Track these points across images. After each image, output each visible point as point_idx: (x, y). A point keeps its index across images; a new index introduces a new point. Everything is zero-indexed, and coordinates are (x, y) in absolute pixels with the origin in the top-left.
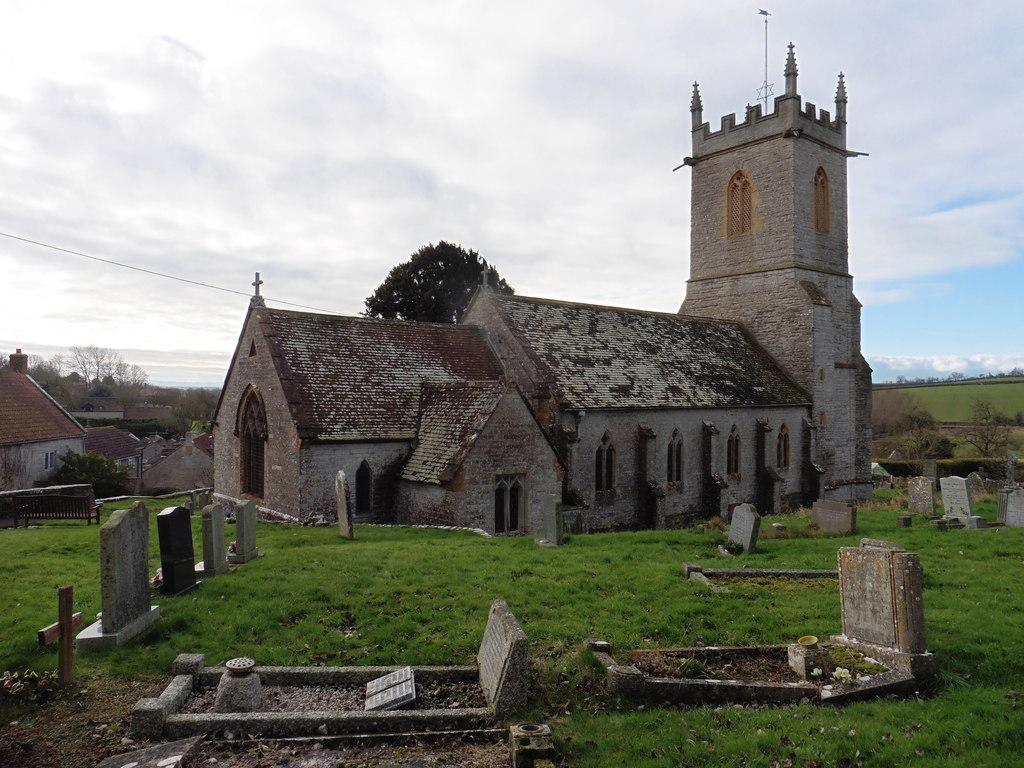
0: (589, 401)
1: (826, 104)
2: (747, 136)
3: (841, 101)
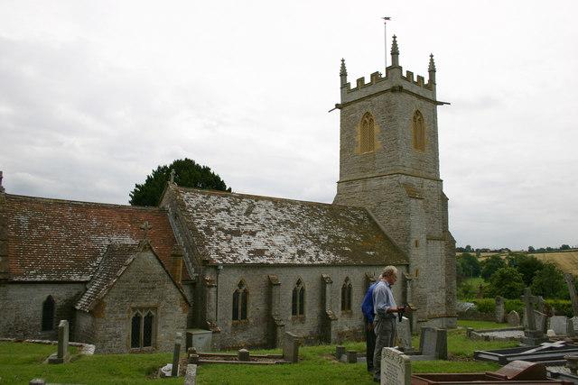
0: (229, 260)
1: (421, 70)
2: (371, 91)
3: (432, 71)
